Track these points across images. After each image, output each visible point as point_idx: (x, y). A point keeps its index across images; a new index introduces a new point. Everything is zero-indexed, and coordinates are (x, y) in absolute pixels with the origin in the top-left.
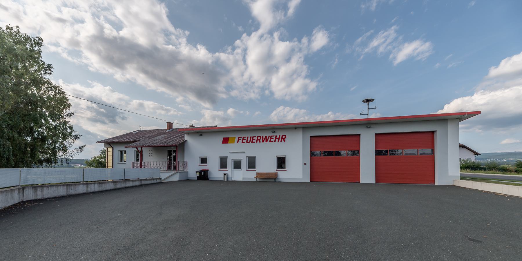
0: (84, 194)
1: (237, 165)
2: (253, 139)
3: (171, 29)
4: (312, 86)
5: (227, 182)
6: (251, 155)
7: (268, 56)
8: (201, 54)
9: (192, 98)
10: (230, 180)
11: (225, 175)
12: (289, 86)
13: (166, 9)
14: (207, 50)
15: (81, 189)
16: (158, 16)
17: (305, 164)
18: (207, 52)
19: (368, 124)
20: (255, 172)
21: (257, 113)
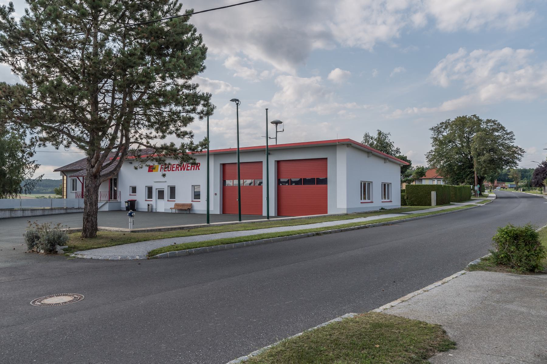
0: (21, 217)
2: (173, 167)
5: (151, 212)
6: (172, 184)
9: (255, 53)
10: (154, 211)
11: (149, 205)
15: (20, 214)
17: (216, 194)
19: (268, 151)
20: (174, 203)
21: (397, 70)
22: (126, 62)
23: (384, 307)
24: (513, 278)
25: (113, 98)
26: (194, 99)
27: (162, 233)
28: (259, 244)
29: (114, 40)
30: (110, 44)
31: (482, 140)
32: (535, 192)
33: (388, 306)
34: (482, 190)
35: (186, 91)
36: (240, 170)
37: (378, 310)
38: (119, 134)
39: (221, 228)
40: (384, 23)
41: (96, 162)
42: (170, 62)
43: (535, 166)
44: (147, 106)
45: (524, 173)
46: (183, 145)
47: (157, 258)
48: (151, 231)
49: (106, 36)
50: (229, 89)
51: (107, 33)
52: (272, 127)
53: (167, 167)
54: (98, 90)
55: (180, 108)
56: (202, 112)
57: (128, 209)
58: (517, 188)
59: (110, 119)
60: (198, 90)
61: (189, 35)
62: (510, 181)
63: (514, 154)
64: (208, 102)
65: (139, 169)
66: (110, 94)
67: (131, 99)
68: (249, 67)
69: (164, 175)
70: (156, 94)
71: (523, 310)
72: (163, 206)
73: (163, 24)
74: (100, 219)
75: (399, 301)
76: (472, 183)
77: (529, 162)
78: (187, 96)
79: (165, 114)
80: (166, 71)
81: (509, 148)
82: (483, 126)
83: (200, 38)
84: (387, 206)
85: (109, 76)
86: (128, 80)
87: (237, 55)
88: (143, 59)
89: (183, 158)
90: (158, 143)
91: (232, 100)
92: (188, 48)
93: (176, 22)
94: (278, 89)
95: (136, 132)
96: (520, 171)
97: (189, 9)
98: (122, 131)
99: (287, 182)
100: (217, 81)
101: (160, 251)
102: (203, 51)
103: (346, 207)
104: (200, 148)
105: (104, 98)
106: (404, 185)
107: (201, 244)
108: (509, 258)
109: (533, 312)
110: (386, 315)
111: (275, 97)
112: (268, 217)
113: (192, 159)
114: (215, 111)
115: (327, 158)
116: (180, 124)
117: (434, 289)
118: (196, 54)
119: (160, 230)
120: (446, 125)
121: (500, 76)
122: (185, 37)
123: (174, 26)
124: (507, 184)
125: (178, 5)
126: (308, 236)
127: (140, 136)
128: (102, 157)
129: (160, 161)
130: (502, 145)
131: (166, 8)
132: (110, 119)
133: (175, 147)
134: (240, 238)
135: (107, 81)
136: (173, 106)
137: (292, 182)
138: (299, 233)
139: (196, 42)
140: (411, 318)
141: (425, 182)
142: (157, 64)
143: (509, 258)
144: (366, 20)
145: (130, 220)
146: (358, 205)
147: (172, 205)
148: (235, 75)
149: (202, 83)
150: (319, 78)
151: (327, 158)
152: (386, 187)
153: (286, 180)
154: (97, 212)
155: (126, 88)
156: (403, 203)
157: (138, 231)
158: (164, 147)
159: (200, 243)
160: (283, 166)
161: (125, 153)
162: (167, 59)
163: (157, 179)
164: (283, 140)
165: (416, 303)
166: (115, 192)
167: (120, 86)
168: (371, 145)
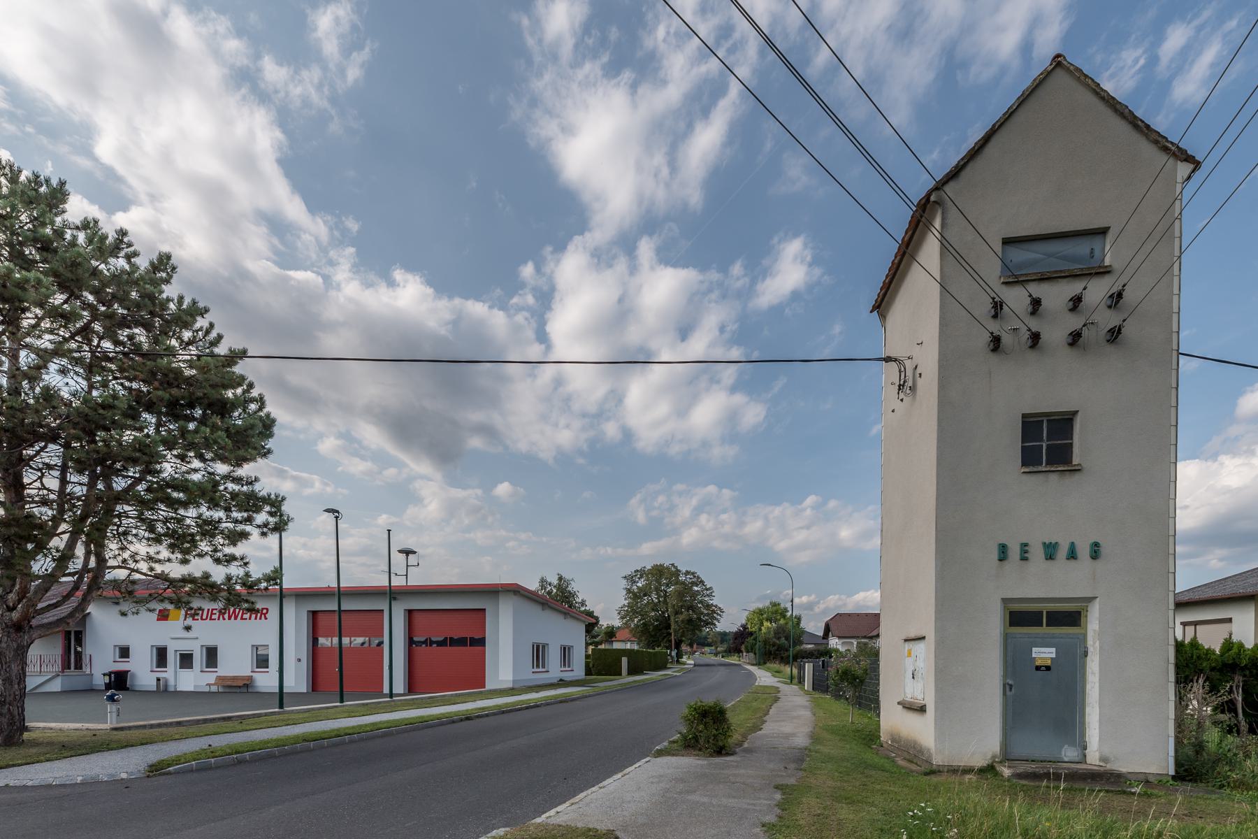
1: (186, 660)
3: (294, 209)
4: (754, 414)
5: (163, 691)
6: (211, 643)
7: (622, 312)
8: (408, 298)
9: (372, 435)
10: (171, 689)
11: (158, 680)
12: (682, 411)
13: (278, 134)
14: (429, 282)
16: (246, 163)
18: (430, 291)
19: (392, 594)
22: (89, 421)
23: (547, 814)
24: (700, 762)
25: (64, 482)
26: (251, 502)
27: (182, 729)
28: (373, 738)
29: (63, 372)
30: (52, 377)
31: (680, 595)
32: (733, 660)
33: (552, 812)
34: (679, 655)
35: (231, 486)
36: (343, 622)
37: (538, 820)
38: (80, 550)
39: (307, 715)
40: (567, 426)
41: (19, 601)
42: (196, 431)
43: (734, 629)
44: (143, 504)
45: (723, 635)
46: (229, 578)
47: (169, 773)
48: (159, 725)
49: (41, 363)
50: (329, 489)
51: (45, 357)
52: (398, 559)
53: (194, 614)
54: (25, 462)
55: (221, 514)
56: (266, 525)
57: (108, 686)
58: (716, 655)
59: (57, 520)
60: (257, 487)
61: (239, 391)
62: (709, 645)
63: (713, 613)
64: (280, 510)
65: (130, 616)
66: (56, 473)
67: (109, 487)
68: (363, 458)
69: (188, 628)
70: (168, 485)
71: (705, 800)
72: (190, 680)
73: (183, 361)
74: (30, 706)
75: (568, 804)
76: (669, 647)
77: (728, 623)
78: (234, 495)
79: (188, 521)
80: (189, 445)
81: (708, 606)
82: (682, 578)
83: (261, 401)
84: (568, 676)
85: (53, 437)
86: (98, 452)
87: (340, 436)
88: (135, 417)
89: (228, 600)
90: (176, 571)
91: (328, 511)
92: (236, 414)
93: (206, 362)
94: (417, 500)
95: (123, 549)
96: (720, 633)
97: (238, 346)
98: (87, 545)
99: (425, 642)
100: (304, 475)
101: (177, 761)
102: (268, 425)
103: (511, 678)
104: (264, 585)
105: (40, 478)
106: (591, 647)
107: (264, 744)
108: (696, 738)
109: (714, 801)
110: (548, 824)
111: (408, 511)
112: (391, 695)
113: (247, 601)
114: (290, 524)
115: (484, 610)
116: (221, 541)
117: (612, 784)
118: (252, 427)
119: (179, 724)
120: (641, 573)
121: (703, 518)
122: (230, 394)
123: (203, 370)
124: (707, 649)
125: (213, 334)
126: (453, 722)
127: (131, 557)
128: (36, 592)
129: (178, 603)
130: (701, 602)
131: (187, 335)
132: (57, 520)
133: (212, 579)
134: (338, 730)
135: (46, 447)
136: (203, 509)
137: (432, 643)
138: (438, 717)
139: (253, 407)
140: (580, 825)
141: (617, 646)
142: (169, 431)
143: (696, 738)
144: (544, 418)
145: (110, 707)
146: (529, 675)
147: (211, 678)
148: (340, 469)
149: (264, 475)
150: (479, 492)
151: (484, 610)
152: (566, 651)
153: (423, 639)
154: (23, 694)
155: (100, 464)
156: (588, 671)
157: (129, 728)
158: (185, 580)
159: (261, 742)
160: (418, 618)
161: (96, 583)
162: (191, 426)
163: (173, 633)
164: (417, 579)
165: (588, 805)
166: (79, 656)
167: (78, 461)
168: (549, 593)
